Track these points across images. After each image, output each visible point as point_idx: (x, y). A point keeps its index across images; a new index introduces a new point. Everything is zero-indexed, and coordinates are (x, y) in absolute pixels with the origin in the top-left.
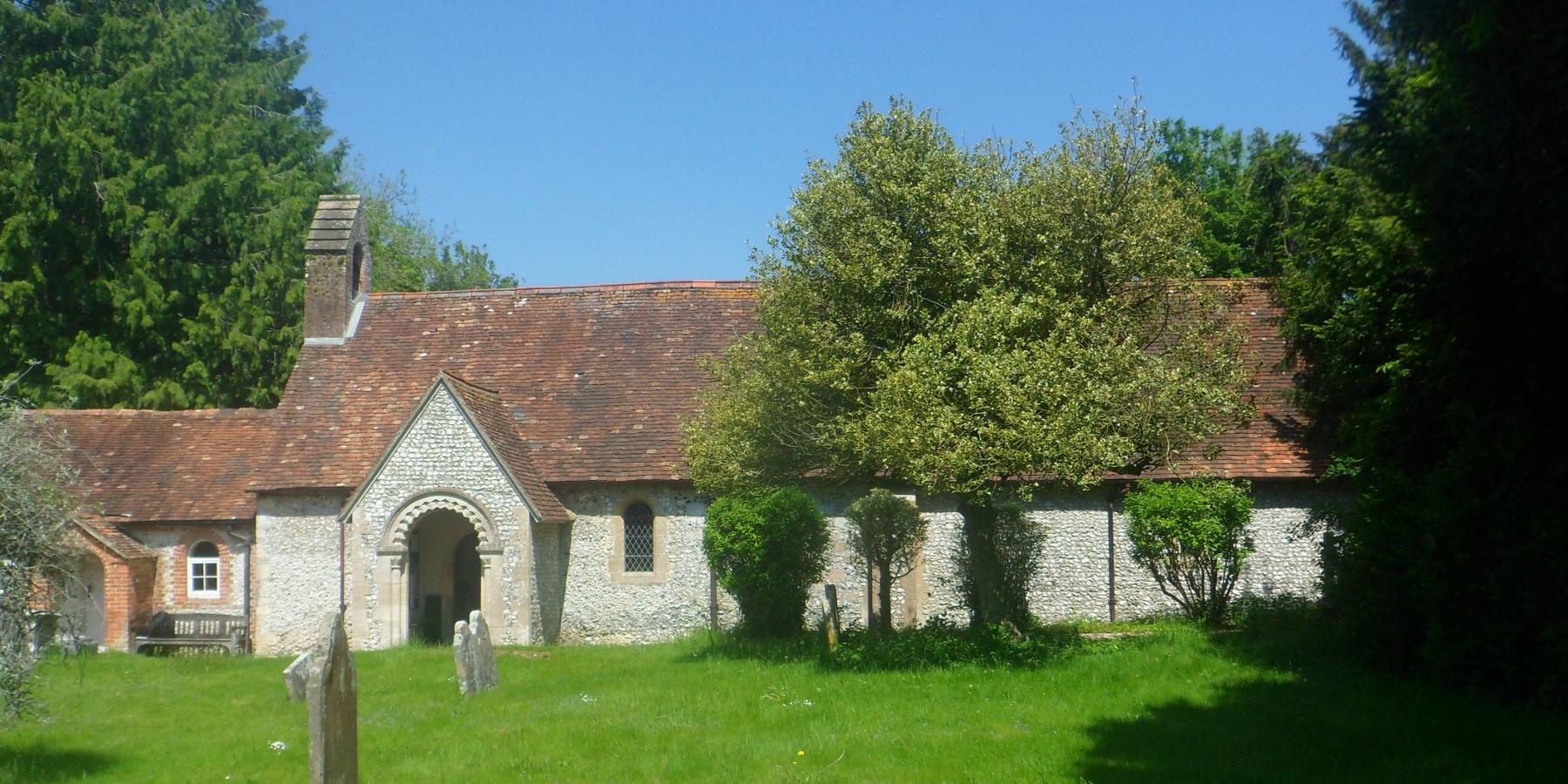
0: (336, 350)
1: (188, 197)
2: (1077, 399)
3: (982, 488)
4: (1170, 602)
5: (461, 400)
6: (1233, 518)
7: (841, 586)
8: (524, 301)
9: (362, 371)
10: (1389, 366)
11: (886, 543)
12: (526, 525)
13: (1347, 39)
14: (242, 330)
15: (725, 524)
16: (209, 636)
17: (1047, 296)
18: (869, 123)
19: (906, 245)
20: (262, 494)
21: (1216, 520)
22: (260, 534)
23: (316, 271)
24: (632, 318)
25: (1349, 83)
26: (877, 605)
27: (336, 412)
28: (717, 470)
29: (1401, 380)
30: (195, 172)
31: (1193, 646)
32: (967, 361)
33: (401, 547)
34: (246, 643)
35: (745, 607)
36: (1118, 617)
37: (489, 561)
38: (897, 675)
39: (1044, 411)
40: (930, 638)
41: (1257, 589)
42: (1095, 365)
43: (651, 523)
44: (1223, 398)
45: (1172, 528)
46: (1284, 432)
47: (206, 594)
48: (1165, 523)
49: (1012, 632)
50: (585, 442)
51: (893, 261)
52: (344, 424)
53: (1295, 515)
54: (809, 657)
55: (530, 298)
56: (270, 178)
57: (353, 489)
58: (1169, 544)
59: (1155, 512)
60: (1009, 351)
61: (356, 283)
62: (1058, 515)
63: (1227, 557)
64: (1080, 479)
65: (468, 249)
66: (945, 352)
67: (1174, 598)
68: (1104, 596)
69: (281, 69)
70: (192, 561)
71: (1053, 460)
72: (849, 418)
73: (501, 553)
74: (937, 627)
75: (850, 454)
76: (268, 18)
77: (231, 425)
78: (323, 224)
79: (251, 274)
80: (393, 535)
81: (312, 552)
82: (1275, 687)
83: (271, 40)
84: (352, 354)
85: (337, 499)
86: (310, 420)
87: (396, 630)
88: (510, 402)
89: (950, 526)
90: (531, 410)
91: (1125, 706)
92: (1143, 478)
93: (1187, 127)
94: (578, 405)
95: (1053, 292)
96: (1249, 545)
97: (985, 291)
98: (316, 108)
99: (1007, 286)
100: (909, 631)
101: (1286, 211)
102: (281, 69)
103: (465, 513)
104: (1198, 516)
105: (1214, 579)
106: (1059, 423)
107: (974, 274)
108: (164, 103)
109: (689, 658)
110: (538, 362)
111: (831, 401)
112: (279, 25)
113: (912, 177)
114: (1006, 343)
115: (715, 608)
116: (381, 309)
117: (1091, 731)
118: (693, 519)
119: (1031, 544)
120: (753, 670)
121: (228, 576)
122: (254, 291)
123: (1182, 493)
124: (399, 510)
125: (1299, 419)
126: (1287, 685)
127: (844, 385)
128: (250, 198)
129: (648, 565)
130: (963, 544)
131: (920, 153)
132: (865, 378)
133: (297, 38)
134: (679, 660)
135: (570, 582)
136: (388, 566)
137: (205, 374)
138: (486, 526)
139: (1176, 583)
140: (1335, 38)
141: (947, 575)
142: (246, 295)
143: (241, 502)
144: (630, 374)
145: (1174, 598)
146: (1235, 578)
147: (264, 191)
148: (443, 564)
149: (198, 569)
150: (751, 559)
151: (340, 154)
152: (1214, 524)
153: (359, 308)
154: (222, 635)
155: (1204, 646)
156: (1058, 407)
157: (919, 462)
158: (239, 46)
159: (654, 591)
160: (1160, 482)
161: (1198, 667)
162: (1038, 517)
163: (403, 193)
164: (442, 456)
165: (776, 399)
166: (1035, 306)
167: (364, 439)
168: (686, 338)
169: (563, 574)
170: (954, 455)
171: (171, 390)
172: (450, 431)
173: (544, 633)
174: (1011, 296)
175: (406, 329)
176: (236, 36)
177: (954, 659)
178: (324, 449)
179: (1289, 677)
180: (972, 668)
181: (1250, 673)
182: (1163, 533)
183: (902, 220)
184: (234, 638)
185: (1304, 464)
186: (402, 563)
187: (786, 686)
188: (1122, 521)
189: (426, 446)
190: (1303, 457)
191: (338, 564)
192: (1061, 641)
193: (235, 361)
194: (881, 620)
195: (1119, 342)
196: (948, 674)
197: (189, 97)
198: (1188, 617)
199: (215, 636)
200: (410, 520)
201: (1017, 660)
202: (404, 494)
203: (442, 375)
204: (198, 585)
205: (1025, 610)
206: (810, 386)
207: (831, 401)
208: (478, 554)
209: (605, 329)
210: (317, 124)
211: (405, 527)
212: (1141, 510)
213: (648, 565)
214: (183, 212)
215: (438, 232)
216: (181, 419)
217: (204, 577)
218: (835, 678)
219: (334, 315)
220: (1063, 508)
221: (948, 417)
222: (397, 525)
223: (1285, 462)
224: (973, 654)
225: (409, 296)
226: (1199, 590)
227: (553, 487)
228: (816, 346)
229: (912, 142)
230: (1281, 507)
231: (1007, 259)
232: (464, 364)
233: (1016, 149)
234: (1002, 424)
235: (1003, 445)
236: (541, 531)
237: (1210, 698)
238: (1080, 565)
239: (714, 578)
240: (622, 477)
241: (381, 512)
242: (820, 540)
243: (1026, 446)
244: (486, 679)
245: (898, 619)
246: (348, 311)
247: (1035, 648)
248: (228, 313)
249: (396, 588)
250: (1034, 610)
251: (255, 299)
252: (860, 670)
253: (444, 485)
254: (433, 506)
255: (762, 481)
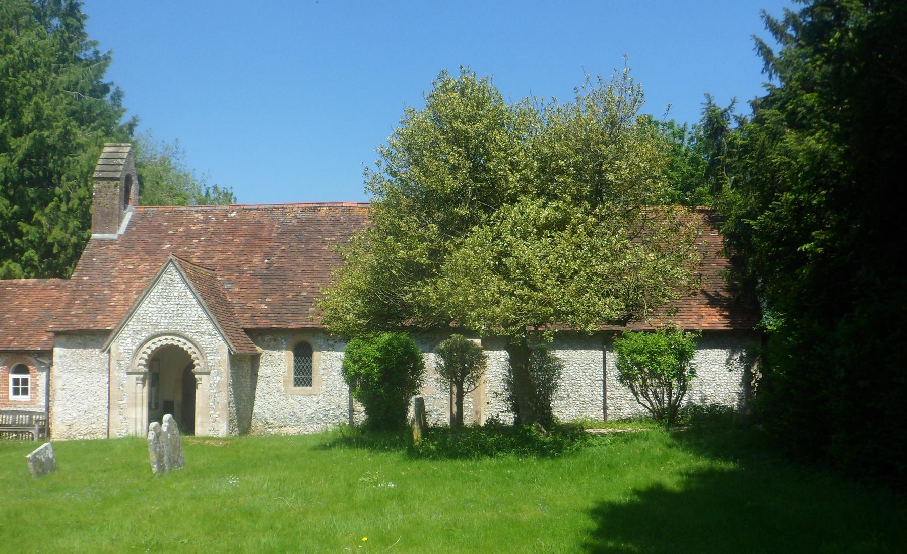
0: (111, 242)
1: (23, 144)
2: (585, 271)
3: (518, 332)
4: (641, 408)
5: (184, 274)
6: (683, 355)
7: (433, 398)
8: (234, 213)
9: (128, 255)
10: (807, 246)
11: (461, 370)
12: (226, 356)
13: (761, 43)
14: (61, 229)
15: (356, 357)
16: (22, 425)
17: (565, 201)
18: (445, 84)
19: (468, 164)
20: (58, 334)
21: (672, 356)
22: (56, 359)
23: (100, 191)
24: (304, 225)
25: (763, 72)
26: (455, 410)
27: (109, 281)
28: (340, 319)
29: (816, 256)
30: (29, 131)
31: (661, 441)
32: (510, 244)
33: (143, 369)
34: (45, 431)
35: (368, 411)
36: (608, 418)
37: (201, 379)
38: (460, 463)
39: (562, 279)
40: (483, 435)
41: (696, 400)
42: (597, 249)
43: (311, 355)
44: (682, 274)
45: (645, 362)
46: (714, 301)
47: (21, 398)
48: (640, 358)
49: (540, 431)
50: (269, 302)
51: (462, 177)
52: (114, 289)
53: (719, 355)
54: (401, 447)
55: (239, 211)
56: (81, 136)
57: (110, 331)
58: (641, 371)
59: (634, 351)
60: (539, 239)
61: (126, 200)
62: (571, 352)
63: (679, 380)
64: (586, 327)
65: (221, 190)
66: (494, 240)
67: (644, 405)
68: (600, 404)
69: (93, 70)
70: (12, 376)
71: (567, 314)
72: (427, 283)
73: (209, 374)
74: (493, 426)
75: (425, 309)
76: (88, 39)
77: (43, 289)
78: (105, 161)
79: (67, 194)
80: (138, 361)
81: (90, 372)
82: (722, 473)
83: (90, 53)
84: (121, 244)
85: (96, 337)
86: (92, 286)
87: (139, 424)
88: (222, 276)
89: (503, 359)
90: (235, 282)
91: (618, 490)
92: (630, 326)
93: (653, 119)
94: (266, 279)
95: (569, 199)
96: (693, 372)
97: (523, 198)
98: (118, 95)
99: (538, 196)
100: (477, 427)
101: (725, 148)
102: (93, 70)
103: (185, 348)
104: (661, 353)
105: (670, 396)
106: (572, 287)
107: (515, 187)
108: (14, 86)
109: (324, 447)
110: (243, 251)
111: (416, 272)
112: (94, 44)
113: (472, 119)
114: (537, 234)
115: (352, 411)
116: (142, 217)
117: (595, 513)
118: (338, 353)
119: (554, 371)
120: (364, 456)
121: (35, 386)
122: (70, 204)
123: (650, 338)
124: (142, 345)
125: (722, 293)
126: (731, 473)
127: (424, 260)
128: (67, 146)
129: (308, 382)
130: (509, 370)
131: (480, 105)
132: (436, 254)
133: (106, 52)
134: (315, 449)
135: (258, 393)
136: (134, 381)
137: (36, 258)
138: (199, 357)
139: (646, 396)
140: (754, 42)
141: (500, 391)
142: (64, 207)
143: (45, 339)
144: (301, 260)
145: (644, 405)
146: (684, 393)
147: (78, 143)
148: (170, 381)
149: (16, 382)
150: (372, 380)
151: (131, 126)
152: (672, 359)
153: (128, 216)
154: (30, 424)
155: (669, 441)
156: (571, 277)
157: (473, 314)
158: (66, 54)
159: (309, 400)
160: (636, 332)
161: (666, 457)
162: (559, 353)
163: (177, 152)
164: (171, 310)
165: (376, 273)
166: (557, 209)
167: (126, 299)
168: (338, 238)
169: (254, 388)
170: (499, 310)
171: (12, 266)
172: (176, 294)
173: (239, 426)
174: (541, 201)
175: (158, 229)
176: (64, 48)
177: (499, 450)
178: (99, 305)
179: (731, 466)
180: (511, 458)
181: (703, 463)
182: (638, 364)
183: (466, 148)
184: (37, 427)
185: (726, 321)
186: (143, 380)
187: (381, 470)
188: (612, 357)
189: (160, 303)
190: (725, 317)
191: (107, 380)
192: (572, 435)
193: (55, 251)
194: (457, 418)
195: (614, 234)
196: (494, 462)
197: (30, 82)
198: (654, 418)
199: (25, 425)
200: (149, 351)
201: (542, 451)
202: (145, 335)
203: (171, 257)
204: (16, 392)
205: (550, 414)
206: (401, 260)
207: (416, 272)
208: (193, 374)
209: (286, 231)
210: (119, 106)
211: (146, 356)
212: (624, 349)
213: (308, 382)
214: (20, 154)
215: (198, 177)
216: (11, 284)
217: (20, 387)
218: (415, 464)
219: (113, 219)
220: (575, 348)
221: (495, 284)
222: (140, 355)
223: (715, 320)
224: (513, 446)
225: (161, 208)
226: (660, 402)
227: (248, 331)
228: (406, 234)
229: (476, 98)
230: (711, 348)
231: (537, 176)
232: (194, 252)
233: (545, 106)
234: (533, 288)
235: (534, 304)
236: (236, 360)
237: (678, 483)
238: (586, 386)
239: (350, 391)
240: (292, 326)
241: (130, 345)
242: (418, 368)
243: (548, 303)
244: (173, 463)
245: (468, 421)
246: (121, 218)
247: (555, 442)
248: (51, 219)
249: (139, 396)
250: (555, 413)
251: (70, 211)
252: (434, 459)
253: (172, 329)
254: (165, 343)
255: (369, 328)
